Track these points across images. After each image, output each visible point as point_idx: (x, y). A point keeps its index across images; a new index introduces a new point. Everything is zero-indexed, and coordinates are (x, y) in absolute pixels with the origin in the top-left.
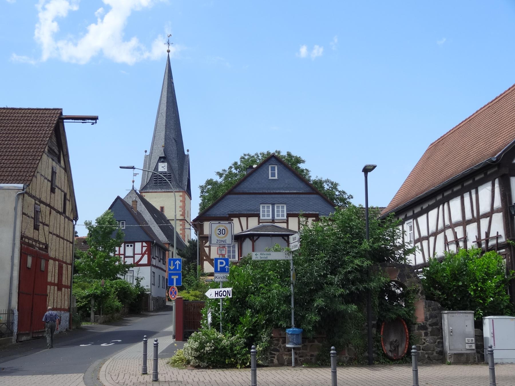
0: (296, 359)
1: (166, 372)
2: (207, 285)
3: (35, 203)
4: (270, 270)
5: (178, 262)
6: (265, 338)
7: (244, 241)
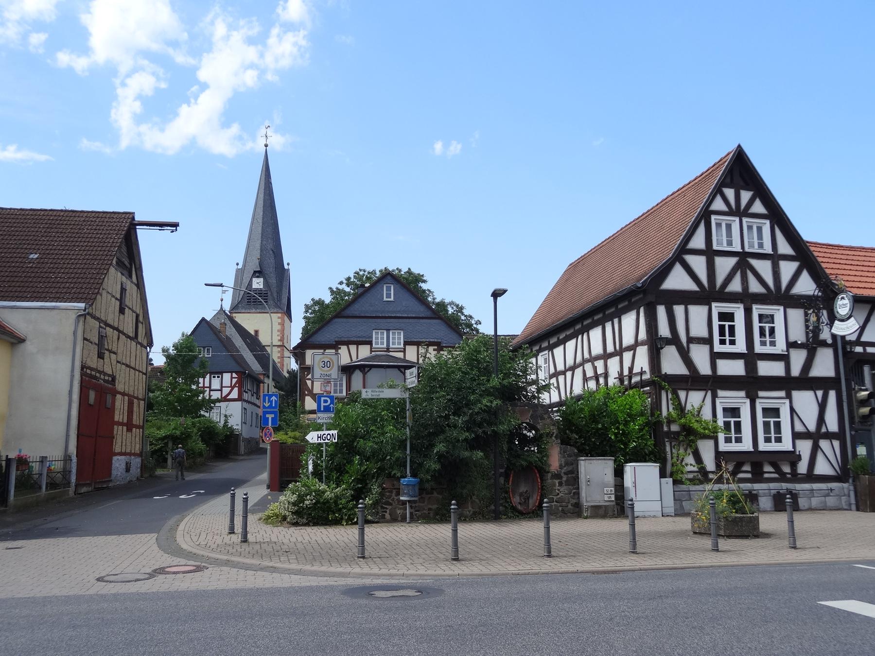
0: (411, 514)
1: (259, 531)
2: (308, 426)
3: (100, 327)
4: (383, 410)
5: (274, 398)
6: (375, 489)
7: (353, 373)
